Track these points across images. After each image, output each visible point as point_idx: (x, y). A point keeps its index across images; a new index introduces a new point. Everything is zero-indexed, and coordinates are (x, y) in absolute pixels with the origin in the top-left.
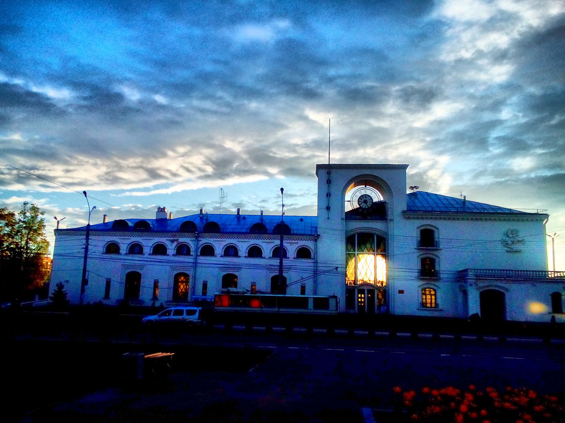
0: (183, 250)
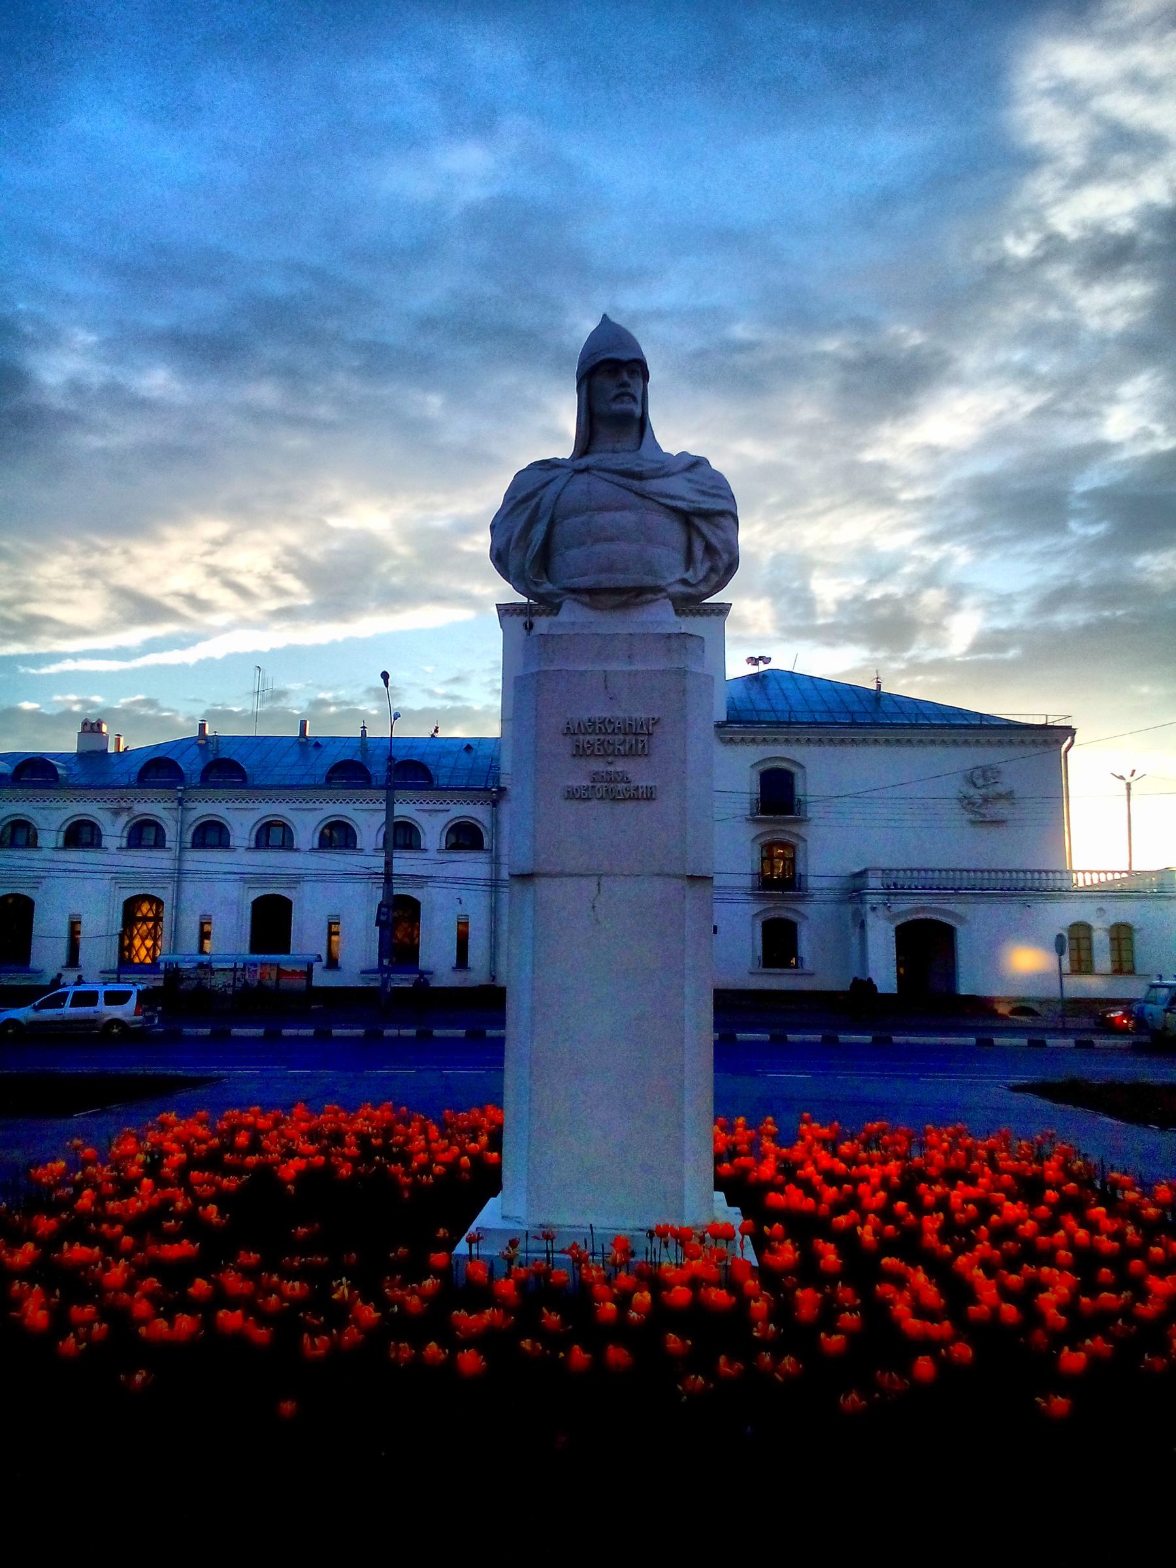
0: (145, 834)
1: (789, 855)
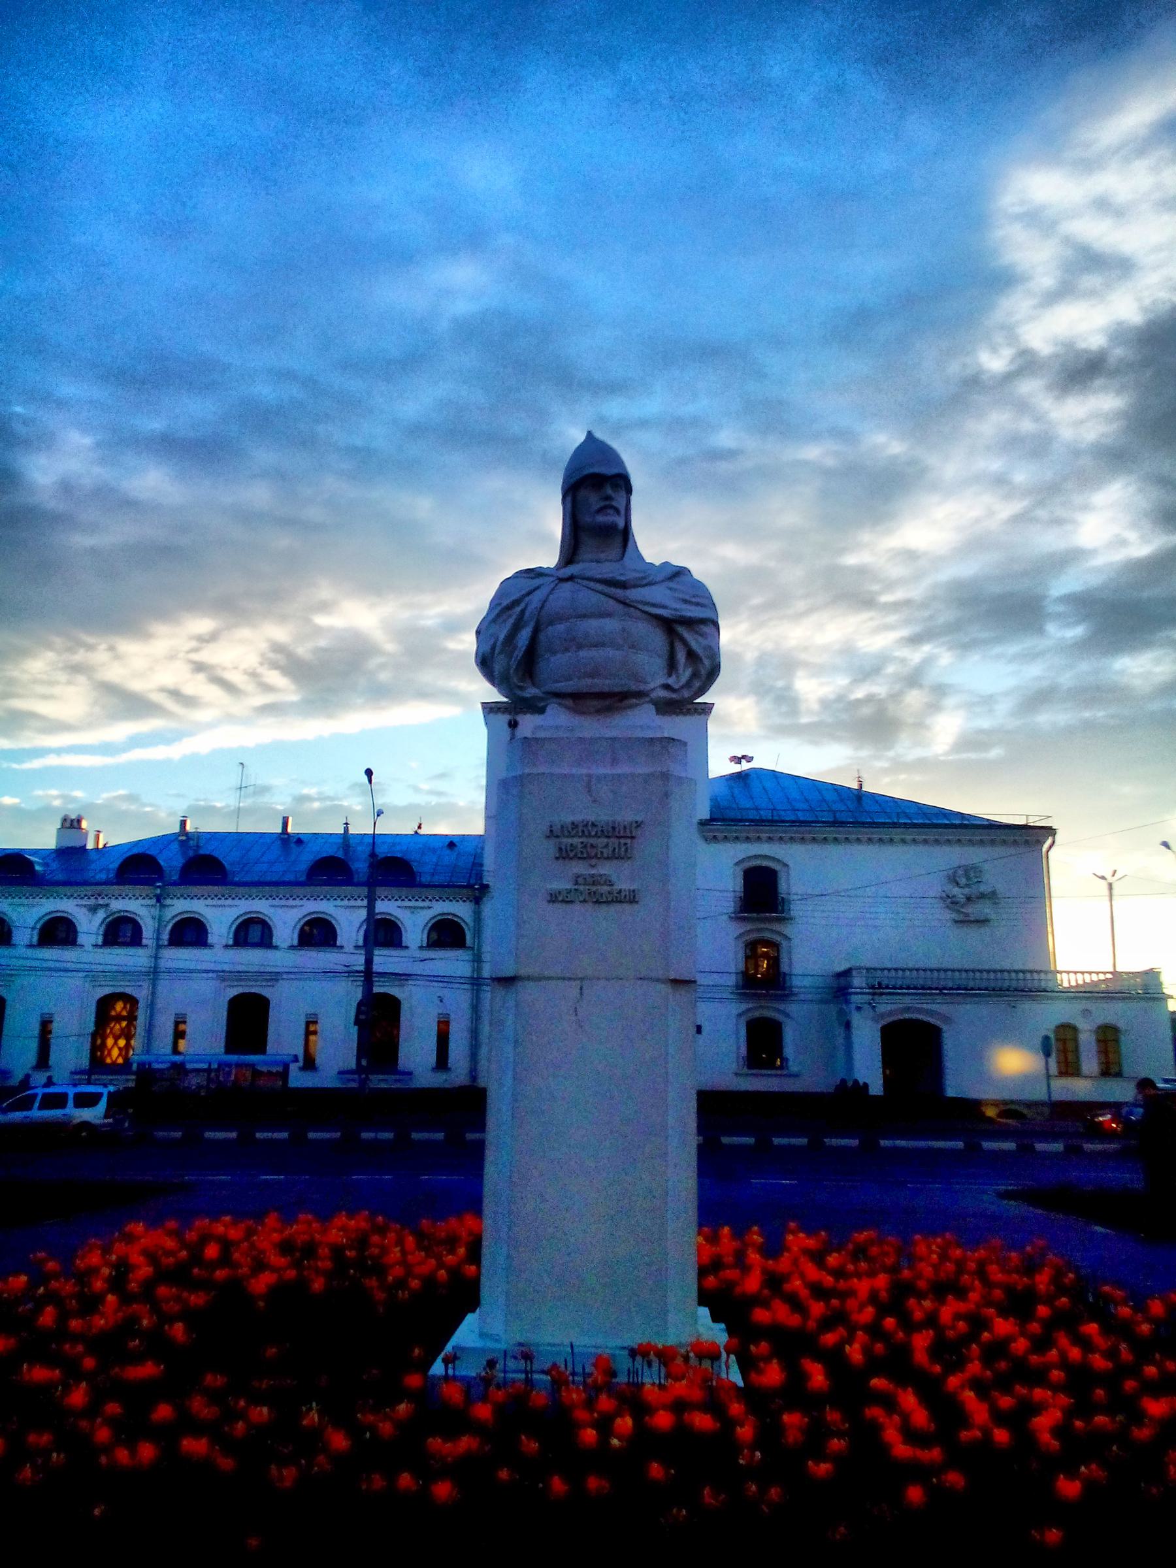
0: (121, 932)
1: (772, 953)
